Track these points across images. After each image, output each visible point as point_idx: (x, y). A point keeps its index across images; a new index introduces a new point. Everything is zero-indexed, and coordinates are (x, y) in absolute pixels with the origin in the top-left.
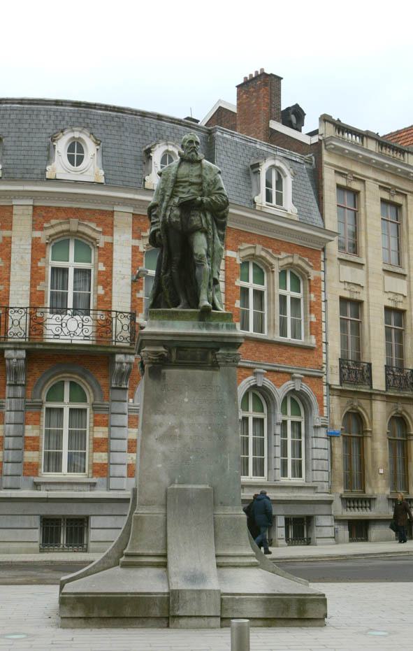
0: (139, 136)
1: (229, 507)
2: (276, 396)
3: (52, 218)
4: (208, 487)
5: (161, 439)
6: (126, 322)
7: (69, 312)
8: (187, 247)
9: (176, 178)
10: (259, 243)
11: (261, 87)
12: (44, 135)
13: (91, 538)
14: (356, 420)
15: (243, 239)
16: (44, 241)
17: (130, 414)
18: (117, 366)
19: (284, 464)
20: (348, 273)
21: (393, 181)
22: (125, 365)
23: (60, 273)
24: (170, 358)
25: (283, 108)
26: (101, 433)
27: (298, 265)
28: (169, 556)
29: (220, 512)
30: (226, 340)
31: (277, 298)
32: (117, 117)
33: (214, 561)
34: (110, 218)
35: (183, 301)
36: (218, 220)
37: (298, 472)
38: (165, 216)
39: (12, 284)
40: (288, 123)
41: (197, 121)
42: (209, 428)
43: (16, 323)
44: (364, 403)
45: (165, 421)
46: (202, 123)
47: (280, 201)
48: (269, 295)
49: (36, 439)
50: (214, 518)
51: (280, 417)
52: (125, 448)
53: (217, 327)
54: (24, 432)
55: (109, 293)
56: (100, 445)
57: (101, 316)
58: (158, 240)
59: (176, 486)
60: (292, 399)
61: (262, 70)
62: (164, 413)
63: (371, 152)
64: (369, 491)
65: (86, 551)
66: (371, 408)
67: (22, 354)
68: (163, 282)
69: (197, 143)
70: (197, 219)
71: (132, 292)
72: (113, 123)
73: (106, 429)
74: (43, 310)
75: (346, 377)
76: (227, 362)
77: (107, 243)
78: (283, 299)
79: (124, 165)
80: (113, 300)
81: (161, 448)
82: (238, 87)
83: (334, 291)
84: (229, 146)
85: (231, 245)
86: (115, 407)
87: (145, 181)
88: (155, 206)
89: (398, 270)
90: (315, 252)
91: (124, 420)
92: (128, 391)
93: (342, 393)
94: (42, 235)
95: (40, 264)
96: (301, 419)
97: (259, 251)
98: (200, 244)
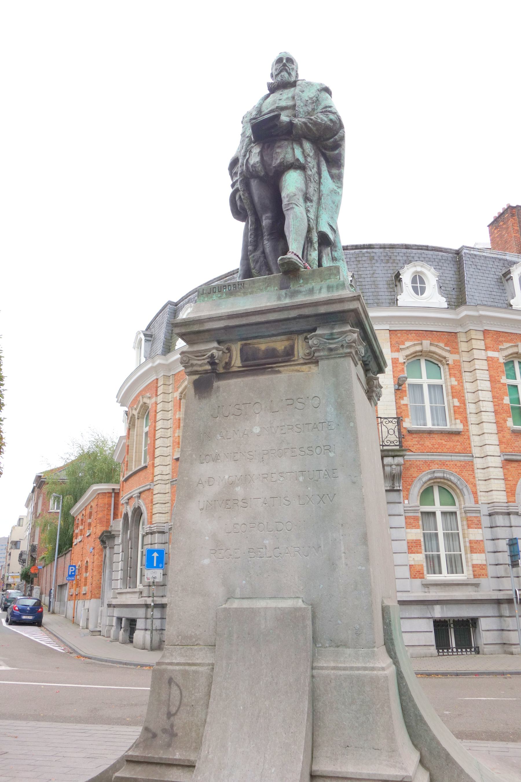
0: (389, 265)
1: (348, 651)
4: (300, 604)
5: (210, 508)
6: (392, 426)
15: (504, 339)
17: (407, 515)
22: (394, 467)
30: (322, 310)
32: (367, 252)
36: (328, 153)
42: (301, 479)
50: (313, 676)
52: (405, 548)
59: (236, 604)
62: (216, 459)
71: (396, 400)
72: (364, 258)
76: (331, 350)
79: (377, 290)
82: (489, 226)
84: (478, 261)
85: (492, 346)
87: (397, 300)
92: (402, 493)
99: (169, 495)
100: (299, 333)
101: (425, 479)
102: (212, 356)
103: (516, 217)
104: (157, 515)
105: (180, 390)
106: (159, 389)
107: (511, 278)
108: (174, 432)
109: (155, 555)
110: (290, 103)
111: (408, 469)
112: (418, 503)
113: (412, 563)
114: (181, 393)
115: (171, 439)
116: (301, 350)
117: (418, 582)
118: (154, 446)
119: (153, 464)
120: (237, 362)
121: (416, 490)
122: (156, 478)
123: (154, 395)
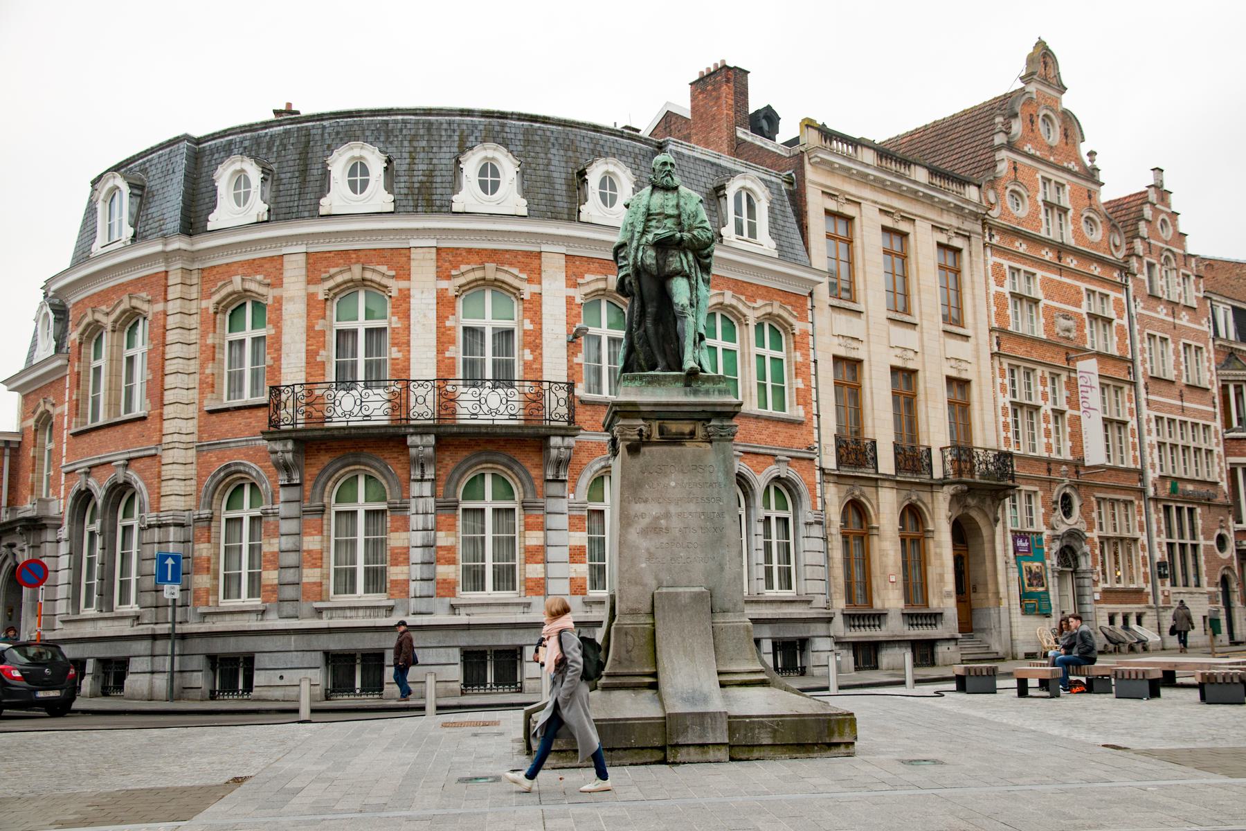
2: (756, 486)
3: (462, 262)
5: (645, 532)
6: (563, 394)
7: (488, 384)
8: (665, 297)
9: (648, 209)
10: (729, 289)
11: (721, 84)
12: (448, 156)
13: (527, 675)
14: (856, 509)
16: (452, 293)
18: (554, 453)
19: (769, 572)
20: (844, 324)
21: (897, 203)
23: (472, 333)
24: (646, 435)
25: (751, 110)
26: (534, 539)
27: (779, 316)
28: (661, 676)
29: (719, 619)
30: (718, 409)
31: (754, 359)
33: (717, 679)
34: (537, 261)
35: (661, 363)
37: (787, 583)
38: (636, 257)
39: (412, 349)
40: (757, 130)
41: (638, 131)
43: (421, 400)
44: (869, 491)
45: (648, 510)
46: (645, 133)
47: (753, 234)
48: (743, 355)
49: (451, 549)
51: (762, 513)
52: (566, 557)
53: (707, 392)
54: (435, 540)
55: (538, 358)
56: (534, 554)
57: (528, 388)
58: (627, 288)
59: (664, 590)
60: (776, 488)
61: (723, 61)
62: (646, 501)
63: (868, 165)
64: (878, 604)
65: (520, 690)
66: (877, 499)
67: (431, 439)
68: (636, 340)
69: (672, 165)
70: (677, 261)
73: (541, 534)
74: (454, 382)
75: (844, 458)
77: (533, 294)
78: (761, 358)
80: (544, 367)
81: (644, 544)
83: (826, 347)
86: (552, 505)
88: (622, 246)
89: (907, 318)
90: (801, 300)
91: (563, 521)
93: (840, 479)
94: (450, 286)
95: (448, 324)
96: (789, 514)
97: (729, 299)
98: (680, 290)
99: (194, 466)
100: (699, 420)
101: (597, 467)
102: (641, 430)
103: (731, 85)
104: (173, 497)
105: (216, 298)
106: (170, 290)
107: (725, 196)
108: (202, 366)
109: (170, 562)
110: (675, 212)
111: (576, 453)
112: (585, 498)
113: (573, 575)
114: (218, 303)
115: (197, 377)
116: (700, 432)
117: (579, 598)
118: (162, 386)
119: (161, 414)
120: (656, 436)
121: (585, 481)
122: (167, 439)
123: (160, 298)
